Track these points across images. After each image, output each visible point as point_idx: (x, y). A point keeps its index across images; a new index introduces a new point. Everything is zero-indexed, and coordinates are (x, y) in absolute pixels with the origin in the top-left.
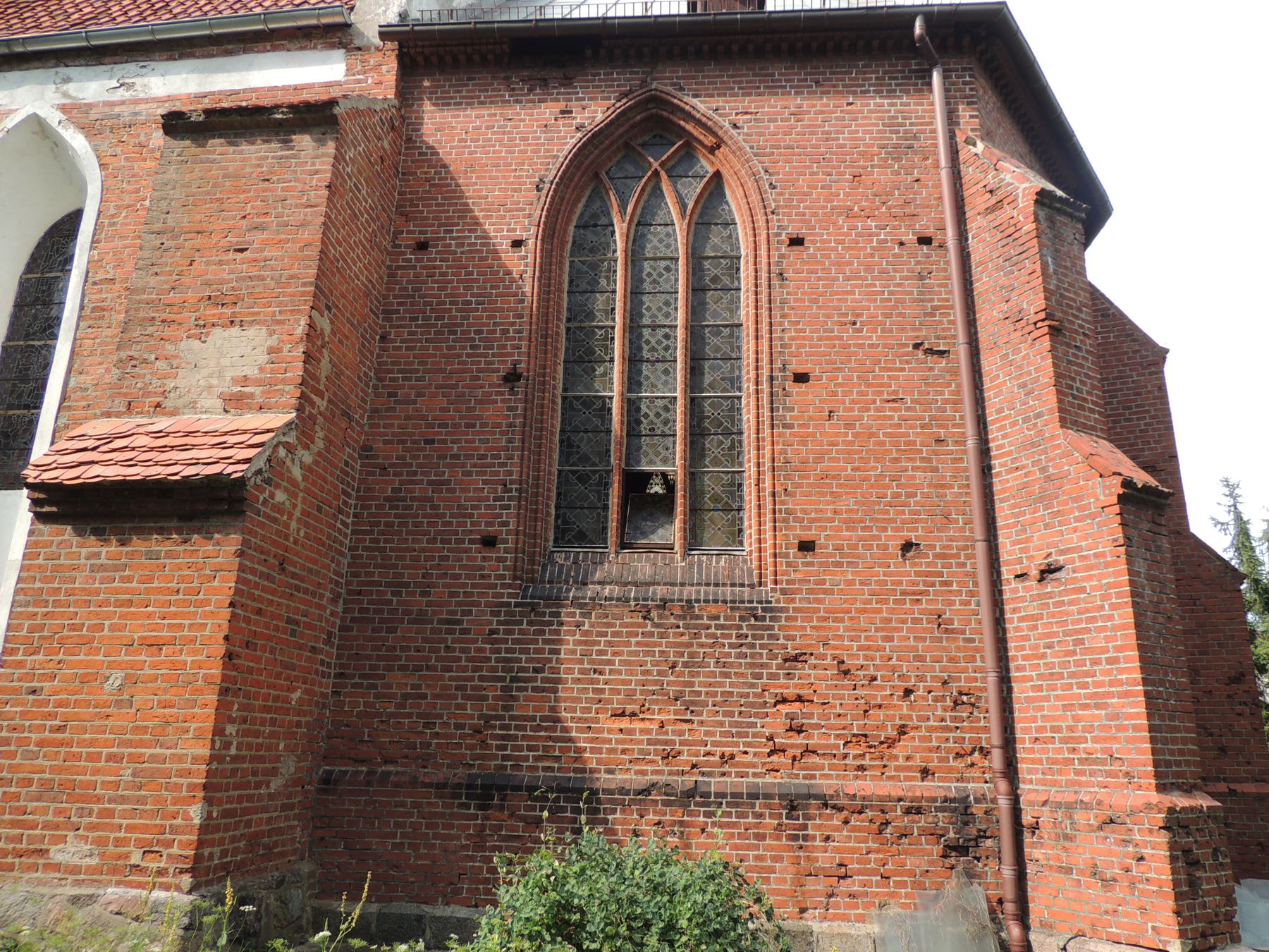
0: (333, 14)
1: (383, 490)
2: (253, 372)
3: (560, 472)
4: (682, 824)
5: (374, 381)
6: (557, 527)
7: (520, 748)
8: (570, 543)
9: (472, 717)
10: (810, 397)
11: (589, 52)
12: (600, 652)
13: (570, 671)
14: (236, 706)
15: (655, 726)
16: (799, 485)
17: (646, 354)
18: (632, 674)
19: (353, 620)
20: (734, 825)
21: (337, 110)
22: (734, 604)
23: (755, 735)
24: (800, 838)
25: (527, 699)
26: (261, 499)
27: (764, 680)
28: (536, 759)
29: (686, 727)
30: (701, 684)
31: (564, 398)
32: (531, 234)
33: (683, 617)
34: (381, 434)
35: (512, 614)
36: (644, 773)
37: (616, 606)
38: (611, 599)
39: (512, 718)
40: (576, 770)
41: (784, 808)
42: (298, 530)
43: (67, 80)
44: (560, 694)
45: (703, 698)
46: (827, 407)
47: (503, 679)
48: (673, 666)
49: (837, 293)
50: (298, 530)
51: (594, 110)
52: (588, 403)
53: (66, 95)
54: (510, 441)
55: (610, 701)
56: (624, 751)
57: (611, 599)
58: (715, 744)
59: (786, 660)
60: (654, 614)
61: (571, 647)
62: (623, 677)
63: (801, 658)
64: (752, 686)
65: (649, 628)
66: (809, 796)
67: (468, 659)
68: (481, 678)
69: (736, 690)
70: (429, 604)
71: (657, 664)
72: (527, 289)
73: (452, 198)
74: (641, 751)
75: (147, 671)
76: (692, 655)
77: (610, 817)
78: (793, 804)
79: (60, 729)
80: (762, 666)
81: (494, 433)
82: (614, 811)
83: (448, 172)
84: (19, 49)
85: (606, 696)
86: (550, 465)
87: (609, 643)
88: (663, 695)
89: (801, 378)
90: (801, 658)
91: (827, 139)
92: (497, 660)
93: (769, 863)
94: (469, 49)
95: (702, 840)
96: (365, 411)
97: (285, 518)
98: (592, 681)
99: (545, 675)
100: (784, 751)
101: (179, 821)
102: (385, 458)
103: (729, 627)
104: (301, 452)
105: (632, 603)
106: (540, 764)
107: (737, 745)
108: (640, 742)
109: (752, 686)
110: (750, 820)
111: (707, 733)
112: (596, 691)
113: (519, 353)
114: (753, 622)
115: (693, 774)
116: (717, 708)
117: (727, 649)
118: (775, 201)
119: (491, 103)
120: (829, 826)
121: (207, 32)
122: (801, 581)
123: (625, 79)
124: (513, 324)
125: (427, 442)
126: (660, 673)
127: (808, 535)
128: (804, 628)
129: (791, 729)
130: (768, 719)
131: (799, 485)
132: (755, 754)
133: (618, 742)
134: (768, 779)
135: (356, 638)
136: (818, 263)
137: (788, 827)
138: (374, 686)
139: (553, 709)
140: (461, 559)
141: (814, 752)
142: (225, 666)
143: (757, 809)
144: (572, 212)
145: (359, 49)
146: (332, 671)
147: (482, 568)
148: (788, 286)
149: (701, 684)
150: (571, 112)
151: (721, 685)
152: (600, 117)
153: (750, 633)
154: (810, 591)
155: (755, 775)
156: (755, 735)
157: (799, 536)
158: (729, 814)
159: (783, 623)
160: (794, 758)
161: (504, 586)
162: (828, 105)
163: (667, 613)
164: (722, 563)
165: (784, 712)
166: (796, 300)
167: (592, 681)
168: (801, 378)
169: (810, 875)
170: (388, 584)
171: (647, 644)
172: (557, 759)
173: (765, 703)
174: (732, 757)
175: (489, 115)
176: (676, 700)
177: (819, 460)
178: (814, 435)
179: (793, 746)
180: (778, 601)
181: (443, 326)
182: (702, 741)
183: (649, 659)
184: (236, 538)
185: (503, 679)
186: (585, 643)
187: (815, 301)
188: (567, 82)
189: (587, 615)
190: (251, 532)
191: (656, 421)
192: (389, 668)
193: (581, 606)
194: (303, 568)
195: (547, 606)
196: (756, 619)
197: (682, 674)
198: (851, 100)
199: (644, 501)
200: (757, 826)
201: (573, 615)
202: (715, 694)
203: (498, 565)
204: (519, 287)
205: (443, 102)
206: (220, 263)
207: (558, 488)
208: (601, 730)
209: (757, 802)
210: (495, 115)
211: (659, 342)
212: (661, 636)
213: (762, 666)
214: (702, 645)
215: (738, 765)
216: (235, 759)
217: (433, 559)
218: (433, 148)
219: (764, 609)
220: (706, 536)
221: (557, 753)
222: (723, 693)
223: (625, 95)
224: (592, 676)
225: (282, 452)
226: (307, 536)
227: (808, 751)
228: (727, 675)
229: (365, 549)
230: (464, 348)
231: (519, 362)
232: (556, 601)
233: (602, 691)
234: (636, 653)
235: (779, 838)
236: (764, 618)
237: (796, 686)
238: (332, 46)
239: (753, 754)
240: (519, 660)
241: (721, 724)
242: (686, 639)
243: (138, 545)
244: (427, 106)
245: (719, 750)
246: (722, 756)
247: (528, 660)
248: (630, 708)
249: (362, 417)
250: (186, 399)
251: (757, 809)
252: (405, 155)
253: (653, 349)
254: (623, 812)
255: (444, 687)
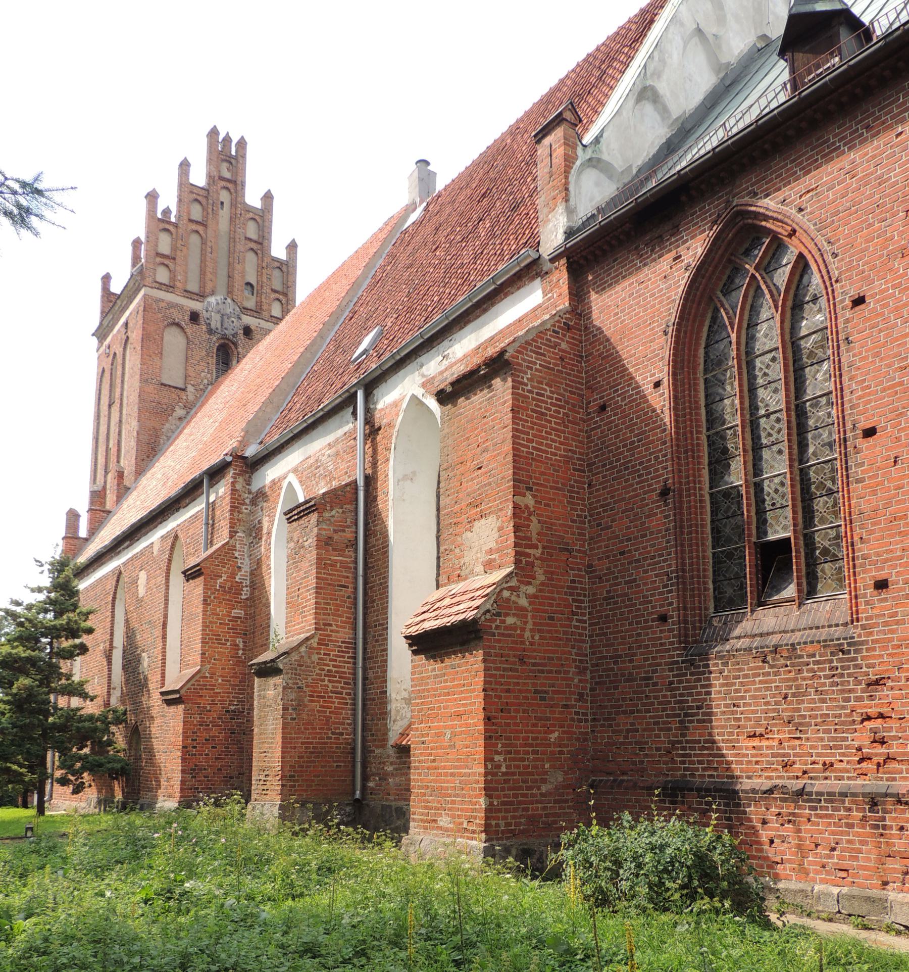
0: (525, 258)
1: (601, 594)
2: (493, 545)
3: (714, 554)
4: (794, 814)
5: (589, 518)
6: (715, 597)
7: (693, 762)
8: (724, 609)
9: (664, 742)
10: (878, 449)
11: (684, 198)
12: (737, 691)
13: (719, 706)
14: (500, 745)
15: (776, 743)
16: (871, 532)
17: (764, 441)
18: (758, 706)
19: (596, 683)
20: (830, 816)
21: (507, 356)
22: (825, 643)
23: (847, 747)
24: (880, 828)
25: (695, 728)
26: (494, 626)
27: (852, 703)
28: (704, 769)
29: (797, 742)
30: (806, 709)
31: (711, 495)
32: (663, 372)
33: (789, 658)
34: (597, 554)
35: (679, 669)
36: (770, 778)
37: (743, 655)
38: (740, 650)
39: (687, 742)
40: (728, 777)
41: (867, 804)
42: (533, 637)
43: (422, 366)
44: (714, 724)
45: (807, 720)
46: (892, 454)
47: (679, 715)
48: (785, 698)
49: (897, 339)
50: (533, 637)
51: (694, 247)
52: (727, 494)
53: (423, 376)
54: (668, 542)
55: (745, 727)
56: (757, 763)
57: (740, 650)
58: (818, 755)
59: (869, 685)
60: (769, 658)
61: (718, 689)
62: (752, 708)
63: (881, 682)
64: (843, 708)
65: (767, 670)
66: (886, 795)
67: (659, 704)
68: (668, 716)
69: (831, 712)
70: (634, 667)
71: (774, 696)
72: (667, 420)
73: (615, 363)
74: (768, 762)
75: (458, 729)
76: (798, 687)
77: (748, 810)
78: (874, 801)
79: (434, 761)
80: (850, 691)
81: (658, 538)
82: (749, 806)
83: (611, 344)
84: (398, 357)
85: (742, 723)
86: (704, 551)
87: (742, 684)
88: (780, 719)
89: (870, 433)
90: (881, 682)
91: (880, 184)
92: (675, 703)
93: (857, 846)
94: (608, 238)
95: (808, 827)
96: (585, 540)
97: (518, 632)
98: (733, 713)
99: (704, 710)
100: (870, 759)
101: (477, 807)
102: (601, 570)
103: (824, 662)
104: (524, 588)
105: (754, 651)
106: (706, 773)
107: (834, 755)
108: (767, 756)
109: (843, 708)
110: (842, 813)
111: (812, 747)
112: (736, 719)
113: (665, 473)
114: (841, 655)
115: (804, 778)
116: (818, 727)
117: (823, 680)
118: (837, 268)
119: (630, 274)
120: (903, 818)
121: (470, 304)
122: (878, 616)
123: (713, 207)
124: (661, 450)
125: (622, 553)
126: (776, 703)
127: (881, 575)
128: (881, 656)
129: (874, 741)
130: (856, 734)
131: (871, 532)
132: (848, 762)
133: (752, 756)
134: (859, 782)
135: (599, 695)
136: (878, 315)
137: (871, 818)
138: (610, 726)
139: (710, 734)
140: (648, 634)
141: (894, 759)
142: (485, 724)
143: (847, 804)
144: (698, 338)
145: (547, 273)
146: (589, 718)
147: (661, 638)
148: (854, 348)
149: (806, 709)
150: (680, 256)
151: (828, 708)
152: (700, 251)
153: (839, 665)
154: (886, 624)
155: (849, 778)
156: (847, 747)
157: (874, 577)
158: (827, 808)
159: (865, 654)
160: (879, 765)
161: (675, 649)
162: (879, 147)
163: (778, 656)
164: (827, 608)
165: (869, 727)
166: (861, 360)
167: (733, 713)
168: (870, 433)
169: (889, 856)
170: (611, 657)
171: (766, 682)
172: (716, 769)
173: (854, 721)
174: (832, 765)
175: (630, 285)
176: (789, 723)
177: (887, 506)
178: (882, 483)
179: (876, 755)
180: (860, 636)
181: (621, 465)
182: (809, 753)
183: (768, 693)
184: (479, 655)
185: (679, 715)
186: (726, 685)
187: (877, 354)
188: (675, 230)
189: (725, 664)
190: (490, 647)
191: (775, 496)
192: (617, 713)
193: (722, 658)
194: (541, 658)
195: (700, 661)
196: (843, 653)
197: (792, 703)
198: (900, 130)
199: (774, 561)
200: (847, 817)
201: (716, 665)
202: (816, 717)
203: (668, 635)
204: (662, 420)
205: (602, 288)
206: (472, 479)
207: (713, 567)
208: (741, 748)
209: (847, 799)
210: (633, 283)
211: (772, 428)
212: (775, 674)
213: (850, 691)
214: (804, 679)
215: (836, 771)
216: (504, 774)
217: (632, 636)
218: (600, 328)
219: (849, 644)
220: (819, 586)
221: (715, 766)
222: (821, 715)
223: (714, 222)
224: (733, 709)
225: (506, 594)
226: (541, 638)
227: (889, 758)
228: (823, 701)
229: (597, 635)
230: (634, 478)
231: (667, 479)
232: (704, 656)
233: (739, 719)
234: (759, 689)
235: (864, 827)
236: (849, 652)
237: (877, 706)
238: (533, 279)
239: (847, 761)
240: (687, 701)
241: (822, 739)
242: (792, 675)
243: (448, 662)
244: (593, 296)
245: (821, 759)
246: (824, 764)
247: (694, 701)
248: (759, 730)
249: (583, 546)
250: (469, 569)
251: (847, 804)
252: (585, 341)
253: (770, 435)
254: (755, 806)
255: (648, 724)
